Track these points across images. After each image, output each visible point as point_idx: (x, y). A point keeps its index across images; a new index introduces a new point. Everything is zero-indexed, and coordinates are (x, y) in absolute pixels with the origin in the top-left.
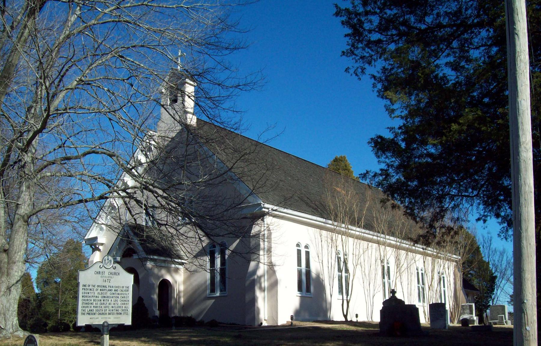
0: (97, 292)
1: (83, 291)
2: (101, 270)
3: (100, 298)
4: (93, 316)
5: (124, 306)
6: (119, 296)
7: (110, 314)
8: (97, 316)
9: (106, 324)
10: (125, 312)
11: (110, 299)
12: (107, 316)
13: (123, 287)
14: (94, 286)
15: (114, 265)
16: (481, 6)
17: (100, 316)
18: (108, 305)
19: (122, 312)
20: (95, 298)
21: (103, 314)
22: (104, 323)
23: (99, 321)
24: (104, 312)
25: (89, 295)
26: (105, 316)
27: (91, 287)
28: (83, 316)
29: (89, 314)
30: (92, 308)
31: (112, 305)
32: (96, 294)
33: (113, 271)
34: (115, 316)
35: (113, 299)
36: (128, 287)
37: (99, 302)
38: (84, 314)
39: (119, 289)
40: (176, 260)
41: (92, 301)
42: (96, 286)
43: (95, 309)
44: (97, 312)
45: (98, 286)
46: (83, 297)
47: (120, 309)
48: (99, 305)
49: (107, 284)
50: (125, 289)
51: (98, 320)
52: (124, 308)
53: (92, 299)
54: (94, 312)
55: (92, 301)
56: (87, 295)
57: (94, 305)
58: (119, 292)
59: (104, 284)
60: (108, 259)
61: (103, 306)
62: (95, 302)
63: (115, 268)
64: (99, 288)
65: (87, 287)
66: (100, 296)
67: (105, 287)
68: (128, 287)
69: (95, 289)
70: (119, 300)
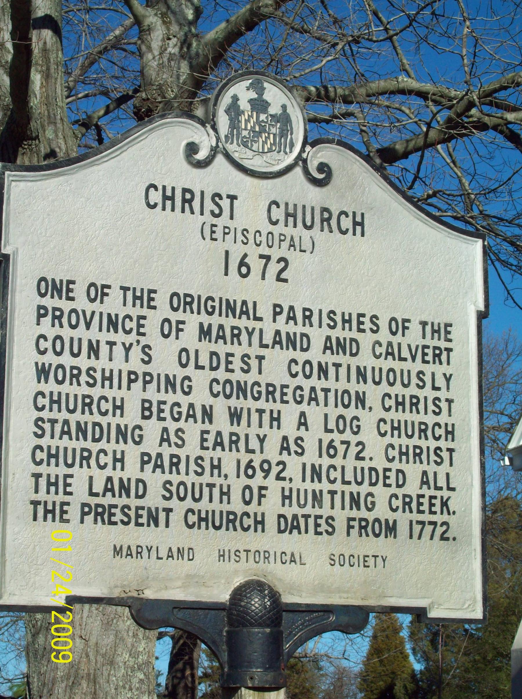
0: (173, 346)
1: (46, 327)
2: (200, 181)
3: (201, 397)
4: (146, 536)
5: (413, 471)
6: (373, 393)
7: (290, 525)
8: (173, 534)
9: (256, 603)
10: (430, 514)
11: (290, 414)
12: (270, 540)
13: (399, 326)
14: (146, 298)
15: (317, 156)
16: (60, 4)
17: (207, 543)
18: (272, 452)
19: (403, 519)
20: (152, 394)
21: (232, 521)
22: (240, 594)
23: (191, 579)
24: (237, 505)
25: (102, 363)
26: (253, 540)
27: (113, 304)
28: (54, 530)
29: (103, 515)
30: (132, 470)
31: (311, 457)
32: (165, 362)
33: (314, 196)
34: (341, 543)
35: (314, 414)
36: (443, 330)
37: (192, 431)
38: (56, 513)
39: (366, 340)
40: (43, 377)
41: (132, 416)
42: (162, 300)
43: (155, 480)
44: (179, 508)
45: (183, 301)
46: (43, 372)
47: (381, 494)
48: (192, 448)
49: (259, 291)
50: (414, 337)
51: (182, 567)
52: (412, 488)
53: (133, 398)
54: (154, 499)
55: (132, 416)
56: (83, 362)
57: (151, 444)
58: (366, 359)
59: (235, 289)
60: (260, 105)
61: (229, 460)
62: (152, 429)
63: (323, 177)
64: (193, 321)
65: (82, 303)
66: (201, 380)
67: (246, 310)
68: (443, 330)
69: (153, 321)
70: (368, 420)
